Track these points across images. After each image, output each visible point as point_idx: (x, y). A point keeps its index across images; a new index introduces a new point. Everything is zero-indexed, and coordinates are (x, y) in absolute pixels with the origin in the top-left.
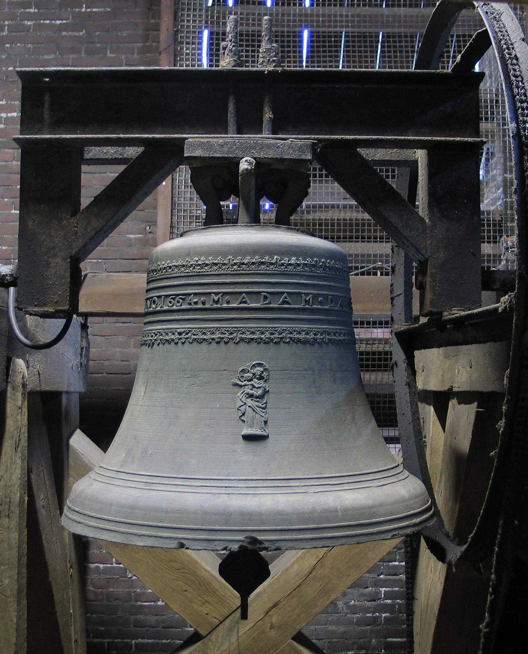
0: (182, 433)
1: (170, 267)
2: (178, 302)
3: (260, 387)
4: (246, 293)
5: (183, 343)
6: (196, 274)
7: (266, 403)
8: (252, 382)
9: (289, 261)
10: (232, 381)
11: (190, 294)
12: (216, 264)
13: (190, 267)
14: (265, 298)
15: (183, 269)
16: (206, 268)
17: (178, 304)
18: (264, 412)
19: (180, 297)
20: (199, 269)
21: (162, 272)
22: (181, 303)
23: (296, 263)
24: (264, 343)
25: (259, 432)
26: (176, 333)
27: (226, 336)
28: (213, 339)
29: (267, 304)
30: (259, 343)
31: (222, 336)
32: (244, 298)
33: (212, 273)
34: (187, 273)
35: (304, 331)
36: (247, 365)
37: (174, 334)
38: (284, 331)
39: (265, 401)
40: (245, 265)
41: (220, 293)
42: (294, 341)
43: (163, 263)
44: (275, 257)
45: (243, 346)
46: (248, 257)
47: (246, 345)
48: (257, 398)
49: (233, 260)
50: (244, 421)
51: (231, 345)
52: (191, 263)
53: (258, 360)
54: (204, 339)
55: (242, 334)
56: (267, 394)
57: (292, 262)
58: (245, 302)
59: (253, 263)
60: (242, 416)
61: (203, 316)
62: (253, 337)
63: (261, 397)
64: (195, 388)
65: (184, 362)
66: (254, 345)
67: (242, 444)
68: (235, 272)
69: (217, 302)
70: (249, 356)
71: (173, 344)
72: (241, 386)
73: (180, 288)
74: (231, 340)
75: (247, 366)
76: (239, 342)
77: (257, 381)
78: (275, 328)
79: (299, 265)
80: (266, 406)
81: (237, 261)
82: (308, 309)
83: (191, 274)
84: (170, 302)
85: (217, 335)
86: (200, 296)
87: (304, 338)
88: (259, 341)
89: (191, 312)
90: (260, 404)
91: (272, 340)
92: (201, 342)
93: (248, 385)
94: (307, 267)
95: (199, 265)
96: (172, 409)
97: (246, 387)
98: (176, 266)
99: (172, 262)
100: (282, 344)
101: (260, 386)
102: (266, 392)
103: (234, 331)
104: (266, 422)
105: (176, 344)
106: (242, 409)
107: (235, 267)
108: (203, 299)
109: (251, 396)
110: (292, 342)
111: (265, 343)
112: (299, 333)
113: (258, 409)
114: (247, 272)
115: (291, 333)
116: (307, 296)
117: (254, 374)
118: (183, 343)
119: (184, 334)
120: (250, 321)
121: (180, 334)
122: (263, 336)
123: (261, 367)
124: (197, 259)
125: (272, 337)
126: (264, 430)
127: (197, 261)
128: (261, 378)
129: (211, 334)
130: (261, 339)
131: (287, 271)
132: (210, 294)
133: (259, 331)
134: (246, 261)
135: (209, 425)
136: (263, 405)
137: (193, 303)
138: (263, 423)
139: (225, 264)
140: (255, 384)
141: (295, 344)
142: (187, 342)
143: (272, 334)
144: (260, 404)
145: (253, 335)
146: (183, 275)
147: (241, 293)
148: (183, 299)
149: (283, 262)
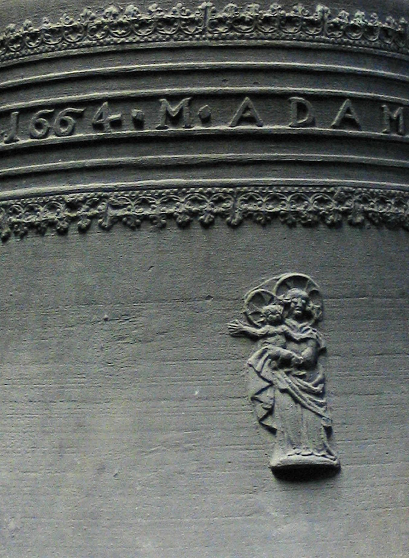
0: (101, 469)
1: (34, 36)
2: (64, 123)
3: (304, 340)
4: (254, 96)
5: (83, 231)
6: (113, 48)
7: (322, 381)
8: (282, 328)
9: (349, 19)
10: (231, 324)
11: (97, 102)
12: (168, 22)
13: (94, 31)
14: (302, 109)
15: (73, 38)
16: (143, 32)
17: (63, 130)
18: (321, 405)
19: (69, 109)
20: (121, 36)
21: (8, 50)
22: (70, 126)
23: (366, 26)
24: (304, 225)
25: (317, 459)
26: (62, 206)
27: (206, 207)
28: (170, 216)
29: (305, 125)
30: (292, 225)
31: (194, 208)
32: (247, 109)
33: (157, 44)
34: (88, 46)
35: (393, 196)
36: (268, 282)
37: (53, 208)
38: (348, 195)
39: (320, 377)
40: (248, 23)
41: (182, 96)
42: (373, 223)
43: (12, 26)
44: (319, 8)
45: (251, 234)
46: (253, 6)
47: (259, 230)
48: (300, 367)
49: (214, 12)
50: (273, 431)
51: (221, 231)
52: (97, 21)
53: (293, 269)
54: (145, 218)
55: (246, 202)
56: (322, 358)
57: (359, 22)
58: (251, 120)
59: (267, 21)
60: (265, 417)
61: (140, 158)
62: (277, 209)
63: (309, 365)
64: (129, 348)
65: (89, 280)
66: (279, 230)
67: (275, 494)
68: (221, 43)
69: (176, 120)
70: (272, 263)
71: (51, 235)
72: (254, 338)
73: (68, 88)
74: (219, 219)
75: (267, 286)
76: (240, 223)
77: (294, 323)
78: (328, 187)
79: (371, 30)
80: (323, 389)
81: (226, 15)
82: (395, 142)
83: (99, 49)
84: (39, 126)
85: (183, 206)
86: (127, 105)
87: (393, 214)
88: (291, 221)
89: (104, 149)
90: (310, 385)
91: (323, 217)
92: (134, 224)
93: (273, 335)
94: (388, 37)
95: (121, 25)
96: (66, 405)
97: (270, 340)
98: (52, 31)
99: (38, 22)
100: (346, 228)
101: (304, 335)
102: (320, 351)
103: (225, 193)
104: (329, 431)
105: (63, 232)
106: (266, 397)
107: (221, 29)
108: (135, 112)
109: (284, 363)
110: (368, 224)
111: (308, 225)
112: (382, 201)
113: (306, 396)
114: (253, 42)
115: (365, 201)
116: (392, 110)
117: (286, 306)
118: (83, 231)
119: (85, 207)
120: (263, 167)
121: (73, 206)
122: (300, 208)
123: (301, 287)
124: (113, 9)
125: (323, 209)
126: (330, 454)
127: (115, 16)
128: (305, 316)
129: (163, 203)
130: (297, 214)
131: (347, 43)
132: (155, 98)
133: (290, 193)
134: (247, 15)
135: (177, 445)
136: (316, 385)
137: (108, 125)
138: (323, 435)
139: (192, 22)
140: (291, 332)
141: (373, 229)
142: (96, 227)
143: (321, 201)
144: (310, 385)
145: (275, 205)
146: (75, 52)
147: (240, 96)
148: (78, 116)
149: (336, 20)
